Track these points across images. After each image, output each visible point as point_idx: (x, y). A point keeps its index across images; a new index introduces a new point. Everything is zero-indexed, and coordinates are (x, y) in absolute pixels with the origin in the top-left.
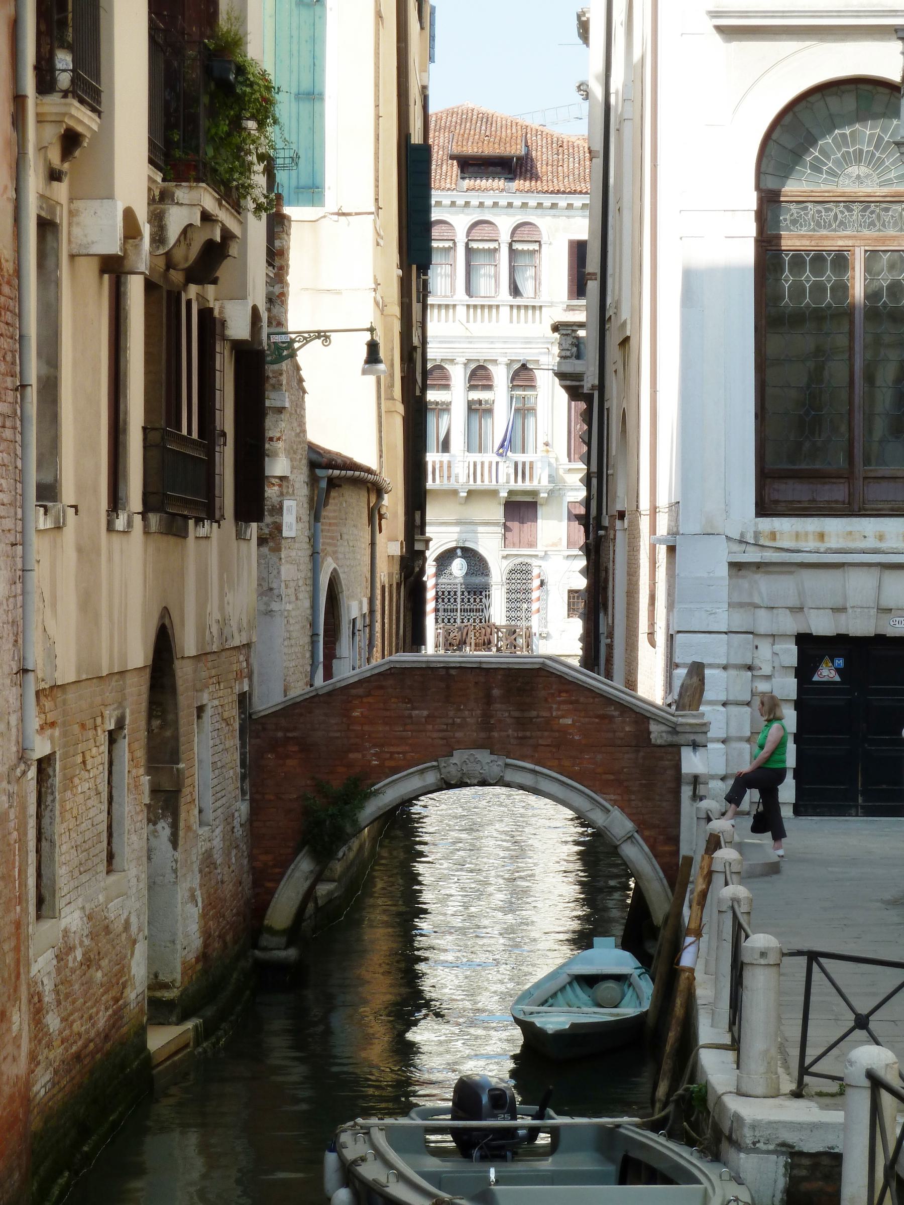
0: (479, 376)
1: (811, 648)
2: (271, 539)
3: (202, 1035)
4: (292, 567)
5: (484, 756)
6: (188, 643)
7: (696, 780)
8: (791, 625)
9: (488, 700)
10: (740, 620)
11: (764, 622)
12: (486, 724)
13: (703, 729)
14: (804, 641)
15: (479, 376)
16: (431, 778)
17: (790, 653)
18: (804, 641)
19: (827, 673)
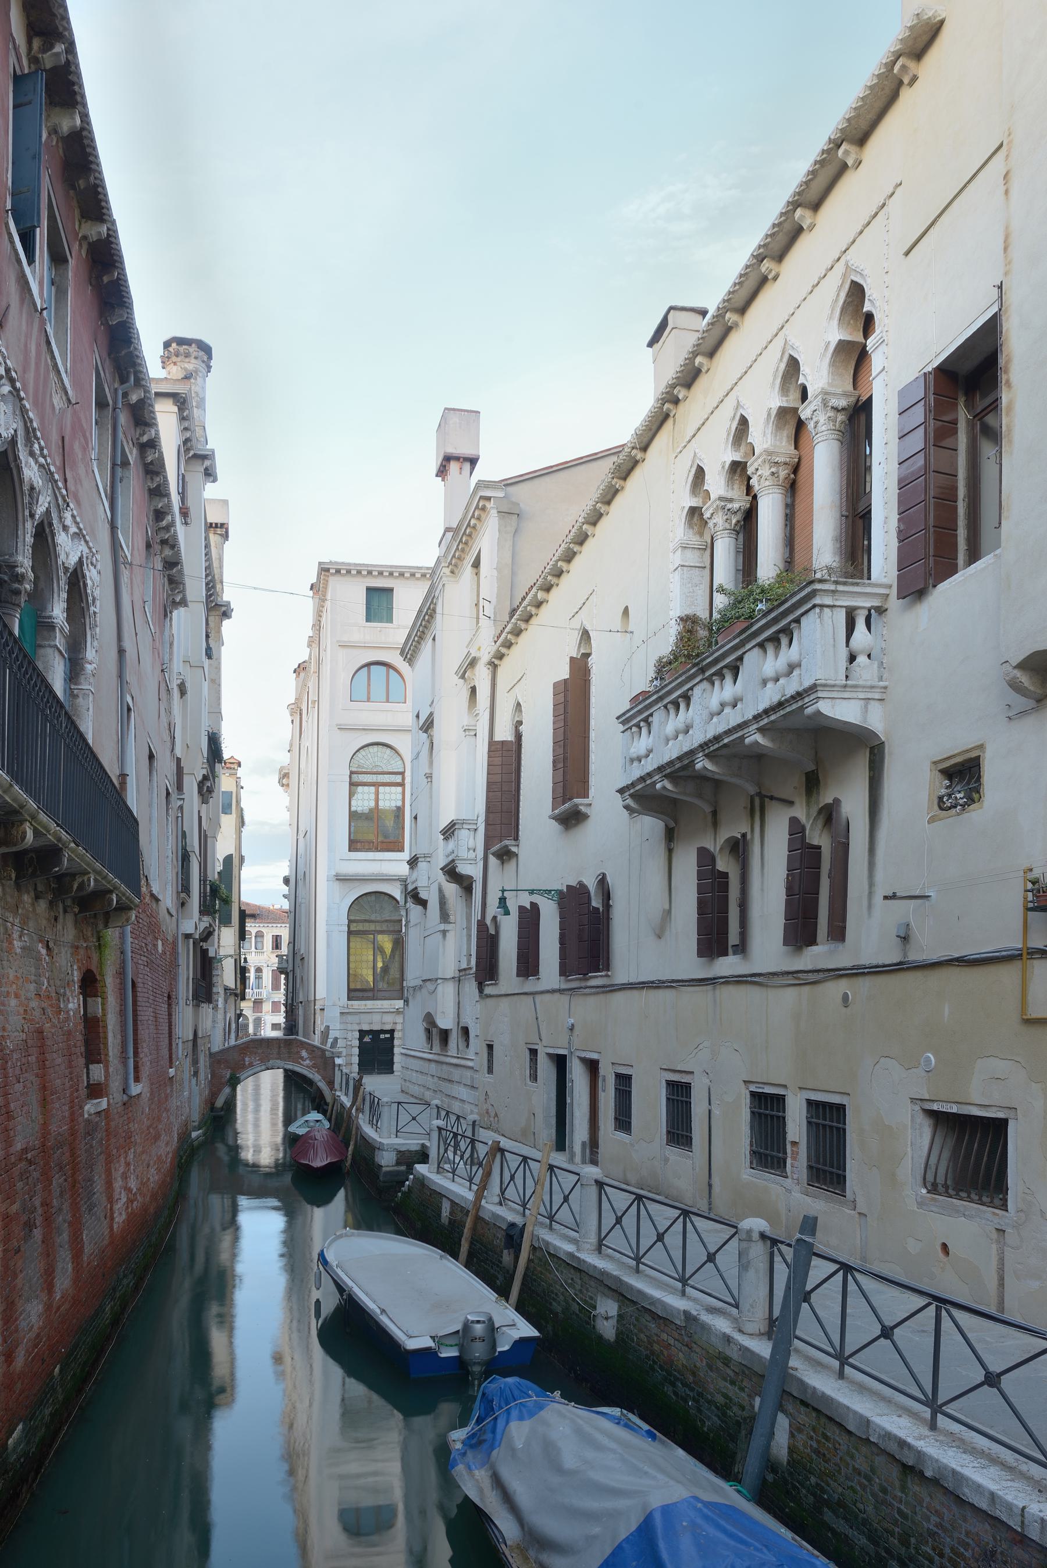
0: (259, 970)
1: (362, 1033)
2: (215, 1008)
3: (204, 1134)
4: (220, 1015)
5: (279, 1061)
6: (200, 1035)
7: (339, 1065)
8: (358, 1028)
9: (280, 1047)
10: (342, 1027)
11: (349, 1027)
12: (279, 1053)
13: (341, 1053)
14: (360, 1031)
15: (259, 970)
16: (263, 1067)
17: (357, 1035)
18: (360, 1031)
19: (367, 1039)
